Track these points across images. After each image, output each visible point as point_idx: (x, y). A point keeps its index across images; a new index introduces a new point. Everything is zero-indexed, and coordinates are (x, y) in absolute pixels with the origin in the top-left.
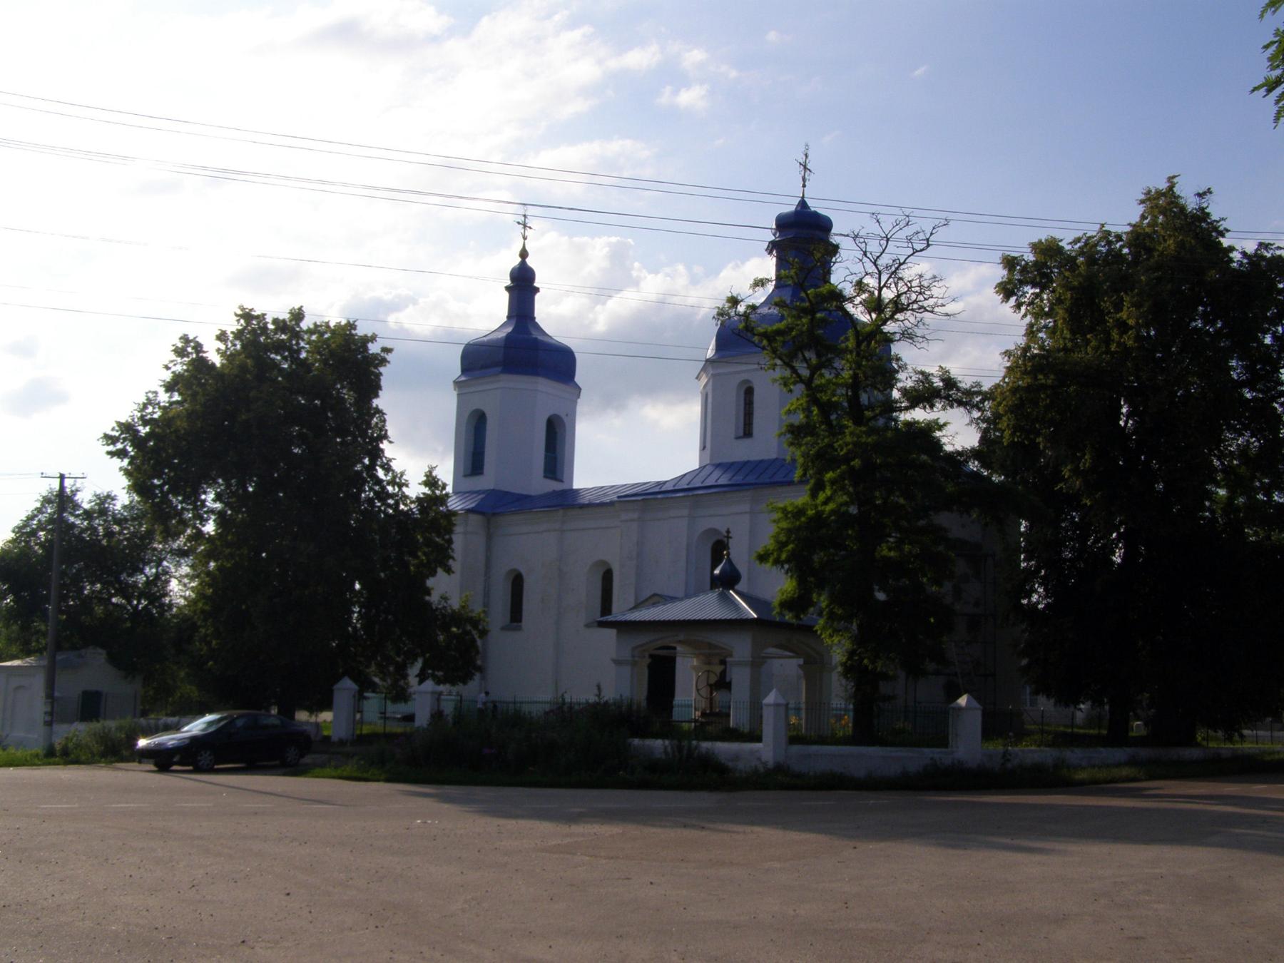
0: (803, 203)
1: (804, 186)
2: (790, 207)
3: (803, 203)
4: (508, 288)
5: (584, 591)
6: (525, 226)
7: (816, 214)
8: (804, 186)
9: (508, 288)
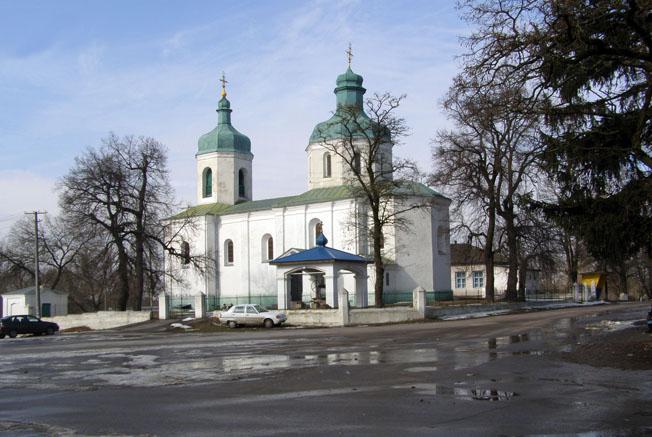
0: (350, 70)
2: (344, 72)
3: (350, 70)
5: (258, 248)
6: (224, 81)
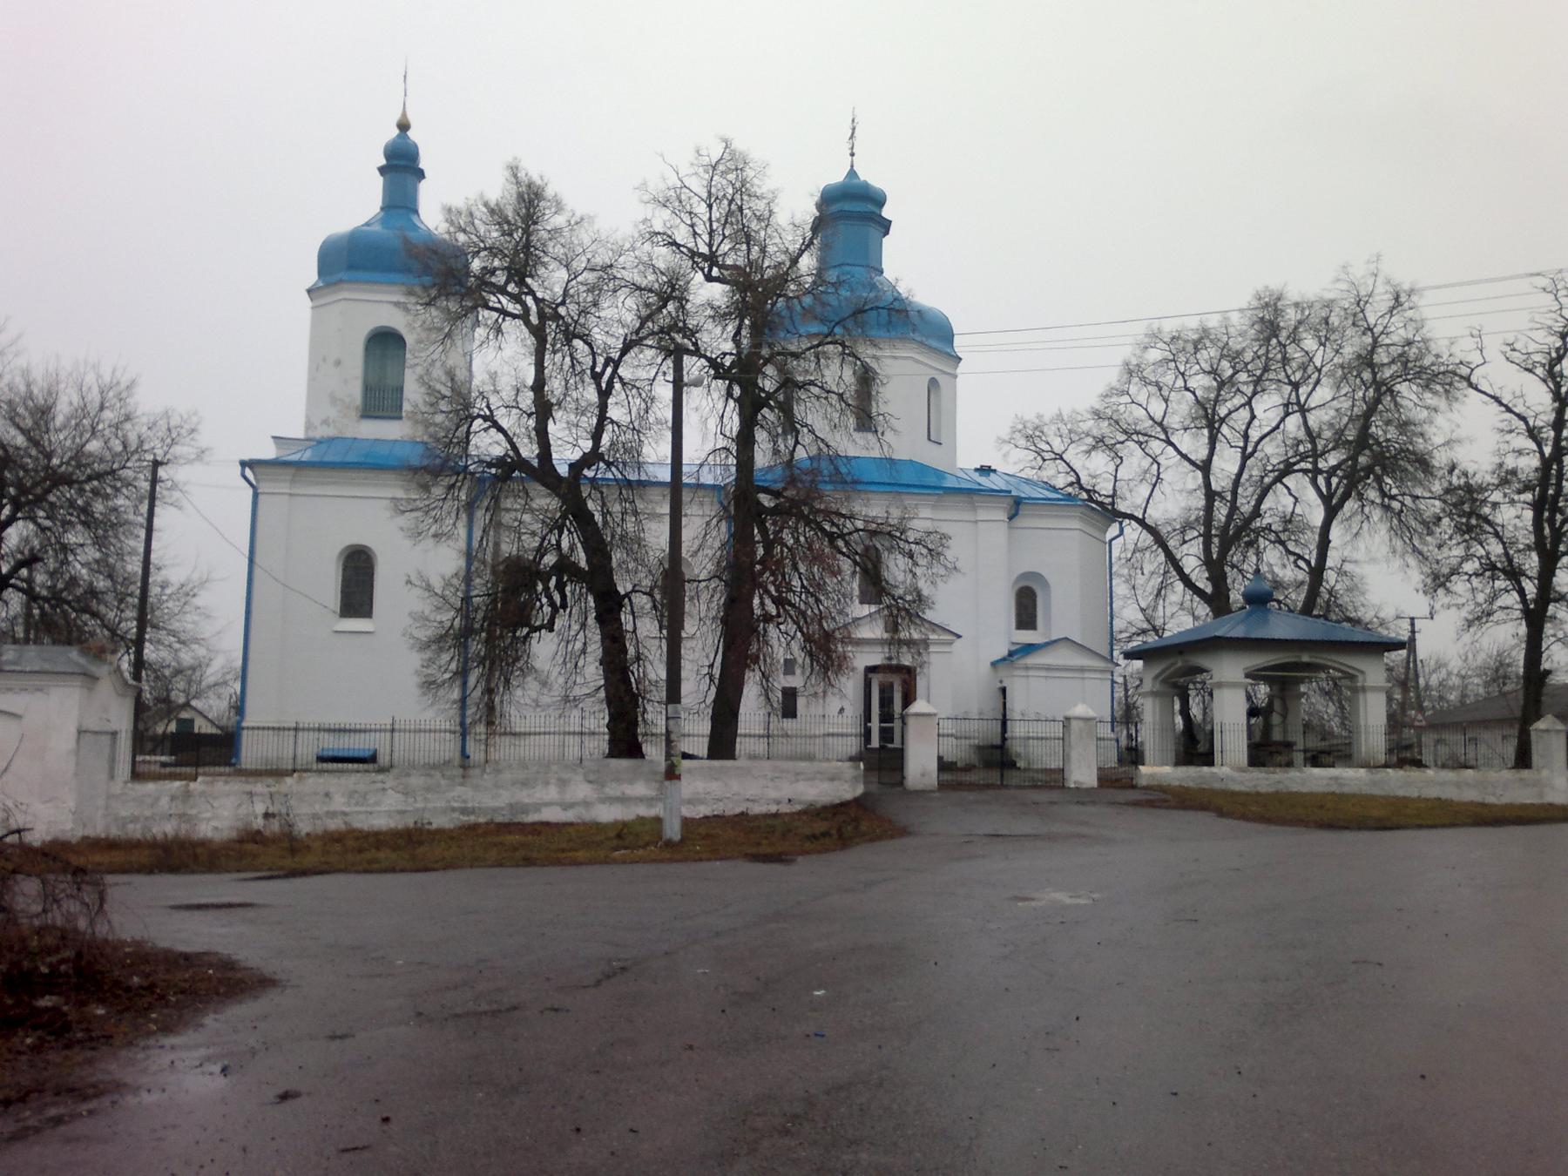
0: (852, 173)
1: (852, 155)
2: (837, 176)
3: (852, 173)
4: (382, 170)
7: (866, 186)
8: (852, 155)
9: (382, 170)
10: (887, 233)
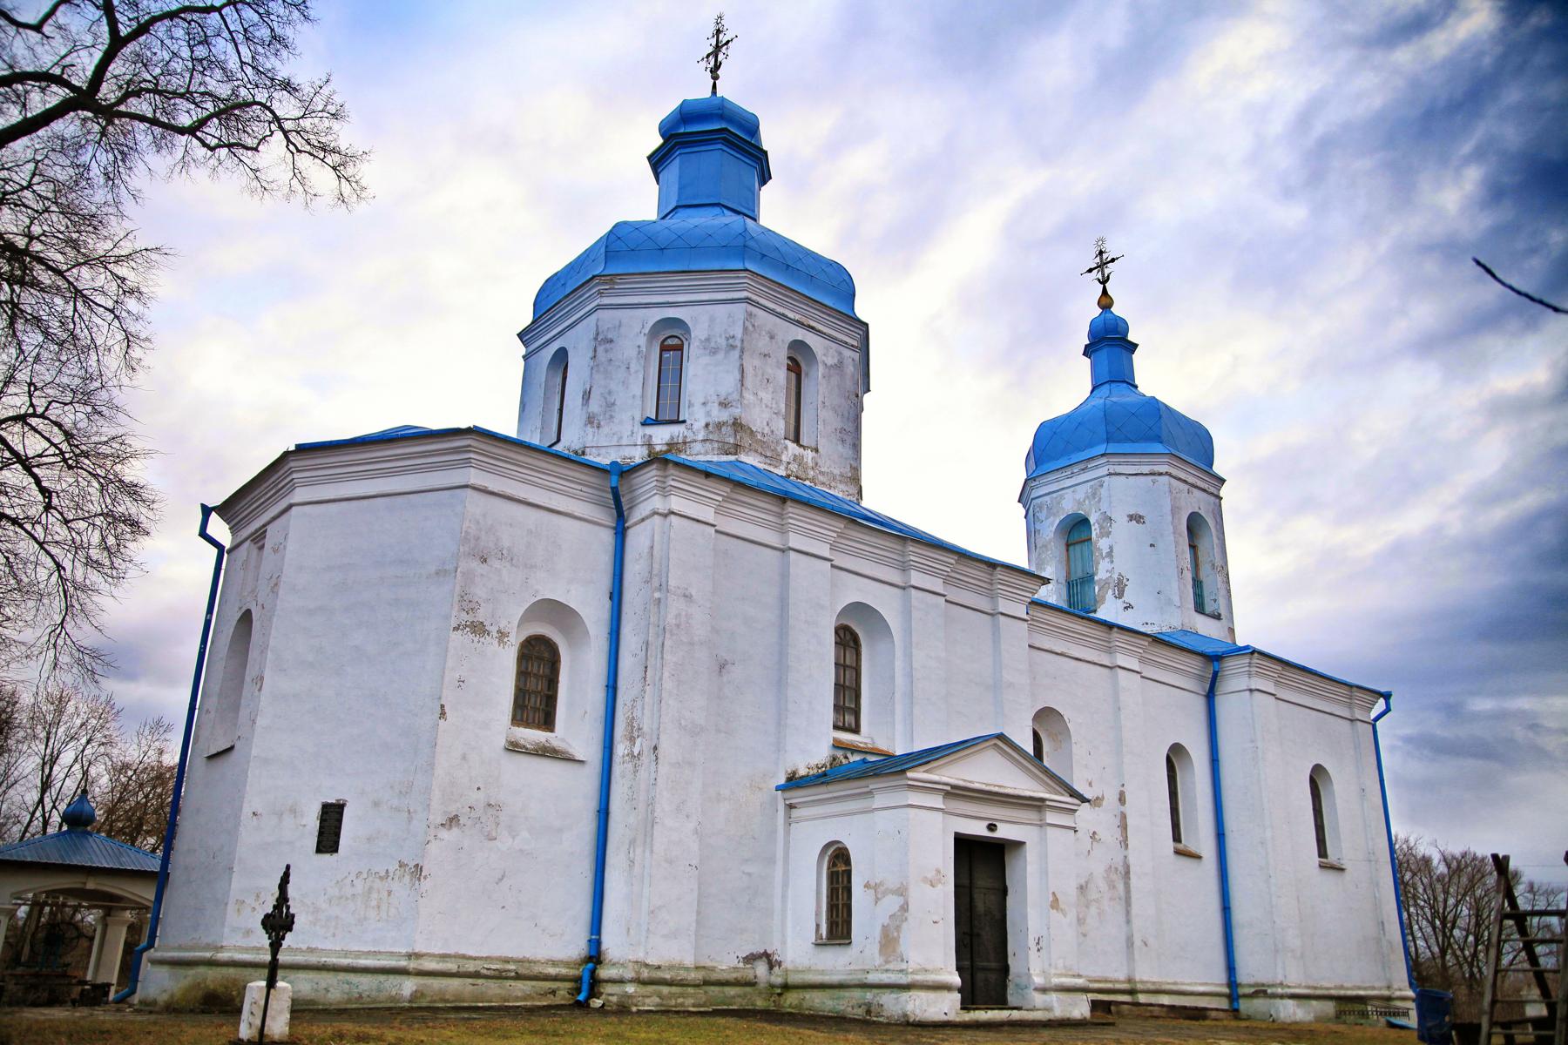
1: (715, 78)
10: (765, 177)
